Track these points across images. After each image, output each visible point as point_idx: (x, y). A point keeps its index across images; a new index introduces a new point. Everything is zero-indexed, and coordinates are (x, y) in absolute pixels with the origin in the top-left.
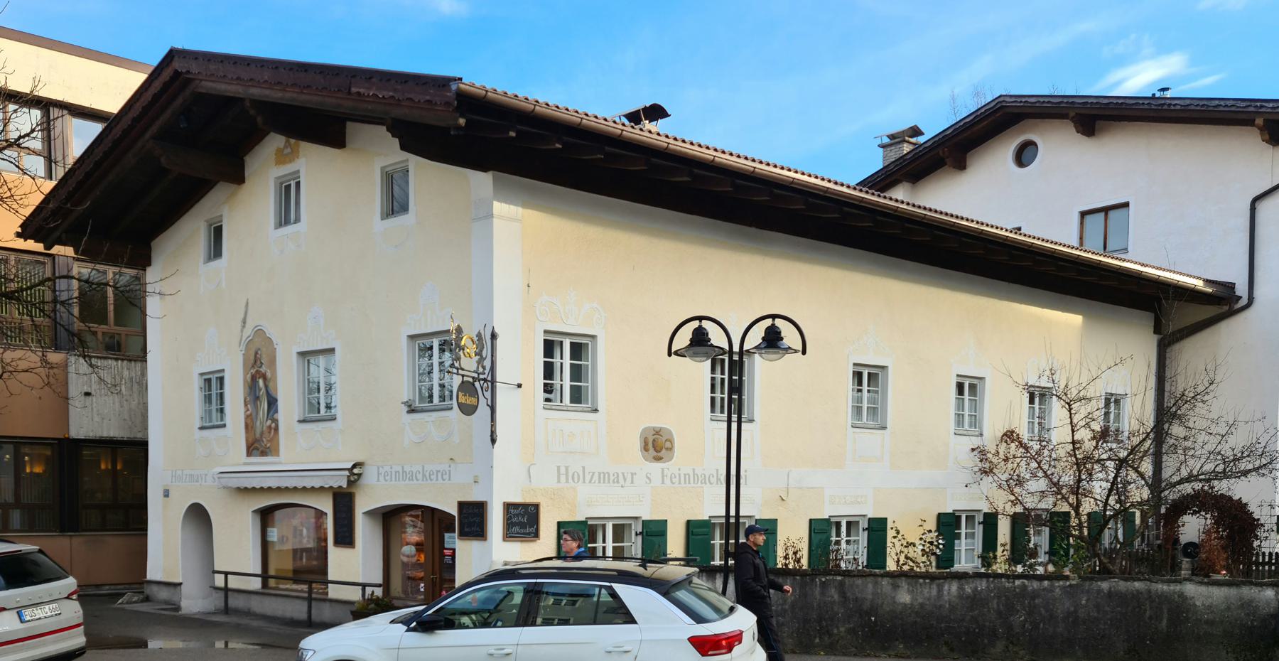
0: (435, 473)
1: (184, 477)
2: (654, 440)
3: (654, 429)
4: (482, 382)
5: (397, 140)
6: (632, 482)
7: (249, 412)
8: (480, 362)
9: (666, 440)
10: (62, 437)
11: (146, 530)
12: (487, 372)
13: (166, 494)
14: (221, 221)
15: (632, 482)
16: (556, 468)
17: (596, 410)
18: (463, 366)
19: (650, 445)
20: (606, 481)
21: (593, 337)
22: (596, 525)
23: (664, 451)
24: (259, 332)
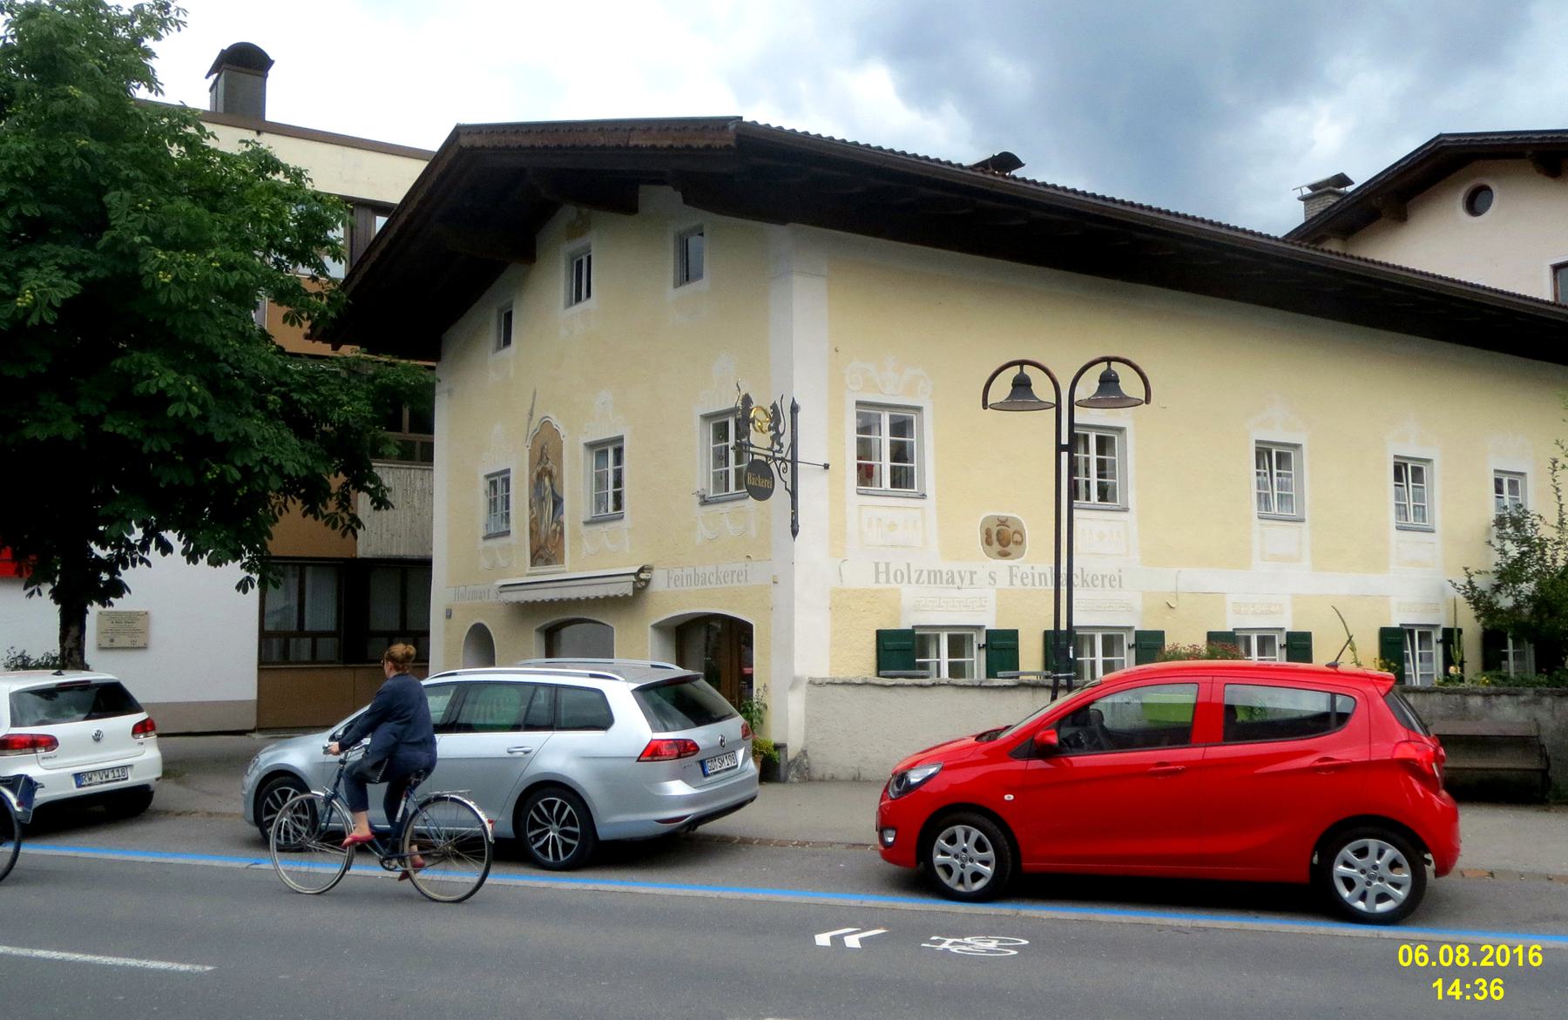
0: (1100, 577)
1: (467, 594)
2: (998, 533)
3: (998, 518)
4: (778, 462)
5: (680, 193)
6: (972, 583)
7: (534, 516)
8: (776, 438)
9: (1014, 533)
10: (349, 557)
11: (428, 661)
12: (785, 450)
13: (449, 615)
14: (511, 306)
15: (972, 583)
16: (874, 565)
17: (923, 496)
18: (752, 442)
19: (994, 537)
20: (938, 581)
21: (918, 409)
22: (929, 635)
23: (1011, 545)
24: (546, 424)
